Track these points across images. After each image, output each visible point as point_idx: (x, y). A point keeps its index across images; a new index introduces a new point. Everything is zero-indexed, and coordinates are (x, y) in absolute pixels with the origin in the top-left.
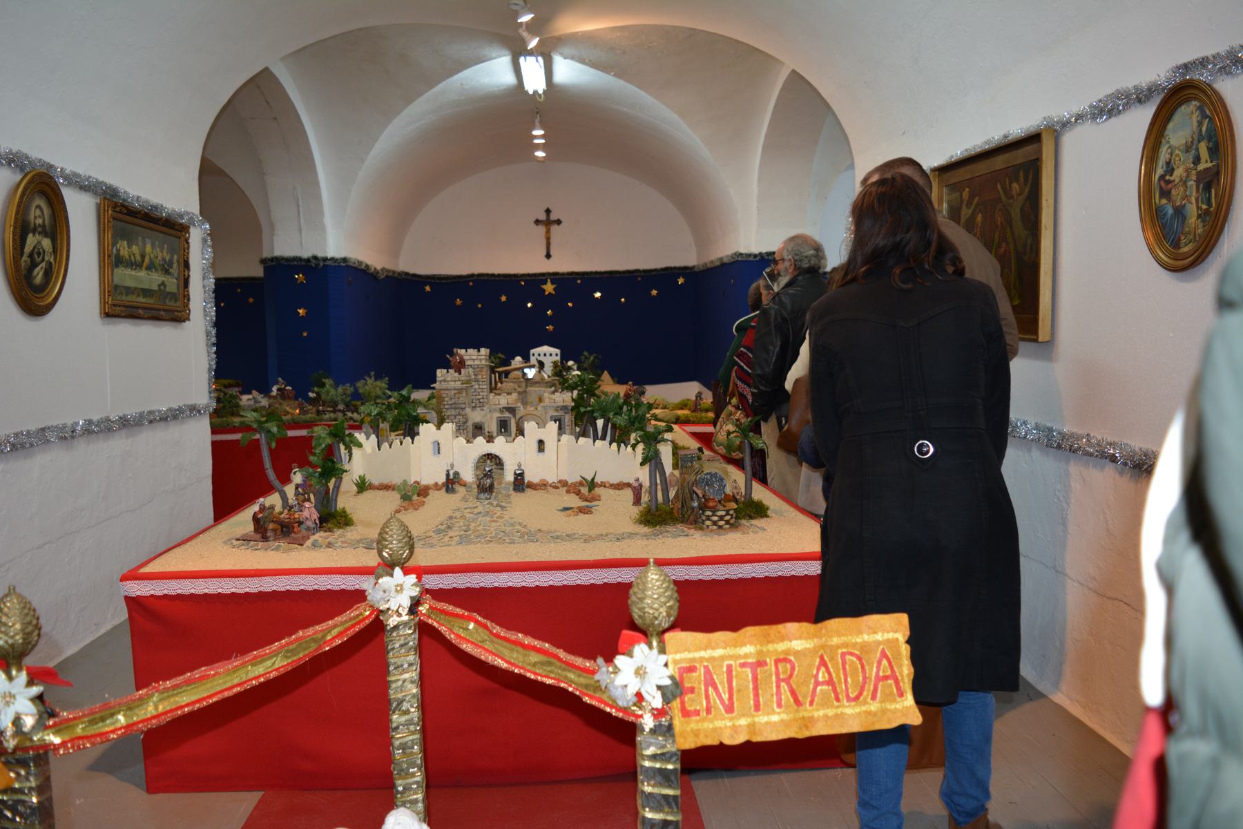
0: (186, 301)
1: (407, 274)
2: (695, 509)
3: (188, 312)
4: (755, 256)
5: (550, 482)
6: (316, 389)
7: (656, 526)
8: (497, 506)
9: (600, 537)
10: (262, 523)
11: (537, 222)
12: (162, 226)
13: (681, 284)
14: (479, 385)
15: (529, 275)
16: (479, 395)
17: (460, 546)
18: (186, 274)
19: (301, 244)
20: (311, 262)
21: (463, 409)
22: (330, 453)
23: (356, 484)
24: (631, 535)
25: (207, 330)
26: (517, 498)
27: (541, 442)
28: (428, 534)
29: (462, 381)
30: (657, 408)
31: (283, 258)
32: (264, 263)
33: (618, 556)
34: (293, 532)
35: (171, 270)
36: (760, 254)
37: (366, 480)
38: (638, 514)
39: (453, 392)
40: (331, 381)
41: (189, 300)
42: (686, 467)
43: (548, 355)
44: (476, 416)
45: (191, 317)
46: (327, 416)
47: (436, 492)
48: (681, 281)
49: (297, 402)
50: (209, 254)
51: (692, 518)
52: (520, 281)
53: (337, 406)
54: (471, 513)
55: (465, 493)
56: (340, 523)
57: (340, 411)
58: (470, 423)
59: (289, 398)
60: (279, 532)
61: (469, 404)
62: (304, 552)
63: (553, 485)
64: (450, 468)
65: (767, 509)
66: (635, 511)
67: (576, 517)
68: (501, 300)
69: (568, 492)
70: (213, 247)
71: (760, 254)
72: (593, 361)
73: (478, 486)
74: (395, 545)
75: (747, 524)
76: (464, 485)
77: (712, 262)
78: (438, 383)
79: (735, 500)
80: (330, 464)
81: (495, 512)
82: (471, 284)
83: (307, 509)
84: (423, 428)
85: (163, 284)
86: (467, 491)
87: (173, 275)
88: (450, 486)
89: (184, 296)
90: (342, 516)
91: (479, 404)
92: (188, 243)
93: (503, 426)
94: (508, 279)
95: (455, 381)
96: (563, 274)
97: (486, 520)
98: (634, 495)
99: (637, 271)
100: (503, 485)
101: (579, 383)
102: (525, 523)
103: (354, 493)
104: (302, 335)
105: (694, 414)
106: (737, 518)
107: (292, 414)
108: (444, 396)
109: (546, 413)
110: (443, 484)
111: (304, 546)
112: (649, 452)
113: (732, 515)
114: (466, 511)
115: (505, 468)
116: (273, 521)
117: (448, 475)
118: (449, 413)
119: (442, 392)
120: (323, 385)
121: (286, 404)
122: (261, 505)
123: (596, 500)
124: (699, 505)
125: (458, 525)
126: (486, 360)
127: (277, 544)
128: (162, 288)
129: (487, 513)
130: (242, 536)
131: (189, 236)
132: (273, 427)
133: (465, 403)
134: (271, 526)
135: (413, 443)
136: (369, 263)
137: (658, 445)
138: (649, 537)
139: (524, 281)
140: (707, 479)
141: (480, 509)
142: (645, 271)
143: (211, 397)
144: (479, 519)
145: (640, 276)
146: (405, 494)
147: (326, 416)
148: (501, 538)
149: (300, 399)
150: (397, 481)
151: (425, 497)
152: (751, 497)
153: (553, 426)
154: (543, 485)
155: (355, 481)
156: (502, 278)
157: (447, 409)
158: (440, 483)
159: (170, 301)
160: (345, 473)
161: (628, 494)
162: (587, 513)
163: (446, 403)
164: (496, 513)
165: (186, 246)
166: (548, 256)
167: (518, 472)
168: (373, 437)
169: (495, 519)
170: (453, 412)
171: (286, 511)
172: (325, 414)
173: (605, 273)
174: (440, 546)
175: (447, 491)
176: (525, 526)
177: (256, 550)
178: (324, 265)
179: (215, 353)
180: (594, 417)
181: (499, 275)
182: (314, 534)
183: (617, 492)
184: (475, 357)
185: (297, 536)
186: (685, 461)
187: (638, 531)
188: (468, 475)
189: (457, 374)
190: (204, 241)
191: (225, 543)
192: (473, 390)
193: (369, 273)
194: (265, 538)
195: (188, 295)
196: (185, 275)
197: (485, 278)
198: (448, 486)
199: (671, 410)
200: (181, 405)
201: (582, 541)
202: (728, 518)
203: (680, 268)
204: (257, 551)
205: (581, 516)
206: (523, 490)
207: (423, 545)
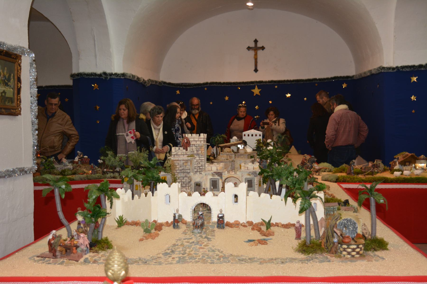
0: (18, 103)
1: (165, 83)
2: (336, 243)
3: (20, 109)
4: (393, 69)
5: (241, 222)
6: (102, 158)
7: (309, 254)
8: (206, 237)
9: (271, 260)
10: (53, 246)
11: (249, 48)
12: (4, 55)
13: (345, 87)
14: (199, 157)
15: (243, 83)
16: (199, 164)
17: (178, 264)
18: (19, 86)
19: (96, 65)
20: (102, 76)
21: (188, 173)
22: (98, 201)
23: (117, 221)
24: (292, 260)
25: (32, 120)
26: (219, 232)
27: (236, 196)
28: (159, 256)
29: (188, 155)
30: (325, 171)
31: (85, 74)
32: (73, 77)
33: (281, 274)
34: (72, 253)
35: (9, 83)
36: (397, 67)
37: (124, 219)
38: (297, 246)
39: (182, 162)
40: (112, 152)
41: (20, 102)
42: (330, 215)
43: (254, 135)
44: (196, 178)
45: (22, 113)
46: (109, 175)
47: (167, 228)
48: (344, 86)
49: (90, 166)
50: (34, 74)
51: (334, 249)
52: (238, 87)
53: (115, 168)
54: (187, 242)
55: (186, 228)
56: (103, 247)
57: (117, 172)
58: (193, 183)
59: (86, 163)
60: (64, 252)
61: (192, 170)
62: (78, 266)
63: (243, 224)
64: (176, 212)
65: (387, 244)
66: (296, 243)
67: (256, 246)
68: (225, 99)
69: (253, 229)
70: (36, 68)
71: (397, 67)
72: (284, 140)
73: (193, 224)
74: (116, 267)
75: (372, 254)
76: (185, 223)
77: (365, 73)
78: (172, 156)
79: (364, 237)
80: (98, 209)
81: (203, 241)
82: (206, 89)
83: (82, 238)
84: (160, 186)
85: (4, 92)
86: (187, 228)
87: (10, 86)
88: (176, 224)
89: (18, 100)
90: (105, 243)
91: (200, 170)
92: (20, 66)
93: (214, 185)
94: (229, 85)
95: (183, 155)
96: (266, 82)
97: (197, 247)
98: (296, 232)
99: (315, 79)
100: (210, 224)
101: (269, 155)
102: (222, 250)
103: (116, 227)
104: (96, 122)
105: (349, 176)
106: (366, 249)
107: (87, 173)
108: (177, 164)
109: (242, 176)
110: (171, 222)
111: (79, 262)
112: (304, 204)
113: (361, 248)
114: (184, 241)
115: (212, 212)
116: (60, 245)
117: (175, 217)
118: (179, 176)
119: (175, 162)
120: (107, 155)
121: (84, 167)
122: (53, 234)
123: (271, 235)
124: (338, 240)
125: (178, 250)
126: (204, 141)
127: (62, 260)
128: (3, 94)
129: (198, 243)
130: (40, 255)
131: (21, 62)
132: (63, 185)
133: (190, 169)
134: (59, 249)
135: (153, 195)
136: (140, 76)
137: (311, 199)
138: (303, 262)
139: (240, 87)
140: (345, 223)
141: (194, 240)
142: (320, 80)
143: (34, 163)
144: (193, 247)
145: (317, 83)
146: (147, 229)
147: (108, 175)
148: (205, 260)
149: (92, 164)
150: (142, 220)
151: (160, 231)
152: (375, 236)
153: (244, 186)
154: (236, 225)
155: (117, 219)
156: (225, 85)
157: (178, 173)
158: (170, 222)
159: (9, 102)
160: (107, 215)
161: (292, 232)
162: (264, 244)
163: (177, 169)
164: (204, 243)
165: (19, 68)
166: (256, 70)
167: (220, 216)
168: (129, 192)
169: (203, 246)
170: (182, 175)
171: (69, 239)
172: (108, 174)
173: (294, 81)
174: (166, 264)
175: (174, 227)
176: (222, 252)
177: (49, 263)
178: (110, 78)
179: (37, 135)
180: (274, 179)
181: (224, 83)
182: (86, 254)
183: (286, 230)
184: (197, 139)
185: (75, 255)
186: (329, 211)
187: (297, 257)
188: (188, 217)
189: (184, 151)
190: (31, 65)
191: (30, 258)
192: (195, 161)
193: (139, 83)
194: (55, 256)
195: (20, 99)
196: (18, 86)
197: (215, 85)
198: (174, 224)
199: (334, 173)
200: (15, 168)
201: (258, 263)
202: (358, 250)
203: (344, 77)
204: (49, 265)
205: (260, 246)
206: (223, 228)
207: (155, 263)
